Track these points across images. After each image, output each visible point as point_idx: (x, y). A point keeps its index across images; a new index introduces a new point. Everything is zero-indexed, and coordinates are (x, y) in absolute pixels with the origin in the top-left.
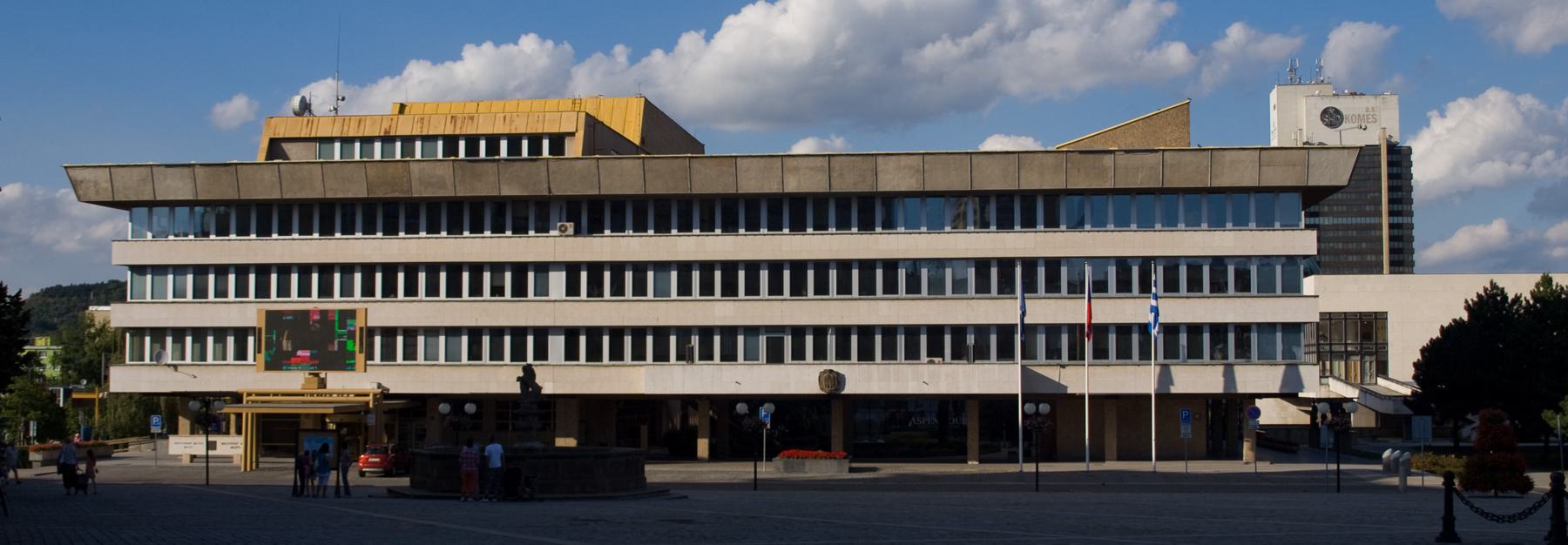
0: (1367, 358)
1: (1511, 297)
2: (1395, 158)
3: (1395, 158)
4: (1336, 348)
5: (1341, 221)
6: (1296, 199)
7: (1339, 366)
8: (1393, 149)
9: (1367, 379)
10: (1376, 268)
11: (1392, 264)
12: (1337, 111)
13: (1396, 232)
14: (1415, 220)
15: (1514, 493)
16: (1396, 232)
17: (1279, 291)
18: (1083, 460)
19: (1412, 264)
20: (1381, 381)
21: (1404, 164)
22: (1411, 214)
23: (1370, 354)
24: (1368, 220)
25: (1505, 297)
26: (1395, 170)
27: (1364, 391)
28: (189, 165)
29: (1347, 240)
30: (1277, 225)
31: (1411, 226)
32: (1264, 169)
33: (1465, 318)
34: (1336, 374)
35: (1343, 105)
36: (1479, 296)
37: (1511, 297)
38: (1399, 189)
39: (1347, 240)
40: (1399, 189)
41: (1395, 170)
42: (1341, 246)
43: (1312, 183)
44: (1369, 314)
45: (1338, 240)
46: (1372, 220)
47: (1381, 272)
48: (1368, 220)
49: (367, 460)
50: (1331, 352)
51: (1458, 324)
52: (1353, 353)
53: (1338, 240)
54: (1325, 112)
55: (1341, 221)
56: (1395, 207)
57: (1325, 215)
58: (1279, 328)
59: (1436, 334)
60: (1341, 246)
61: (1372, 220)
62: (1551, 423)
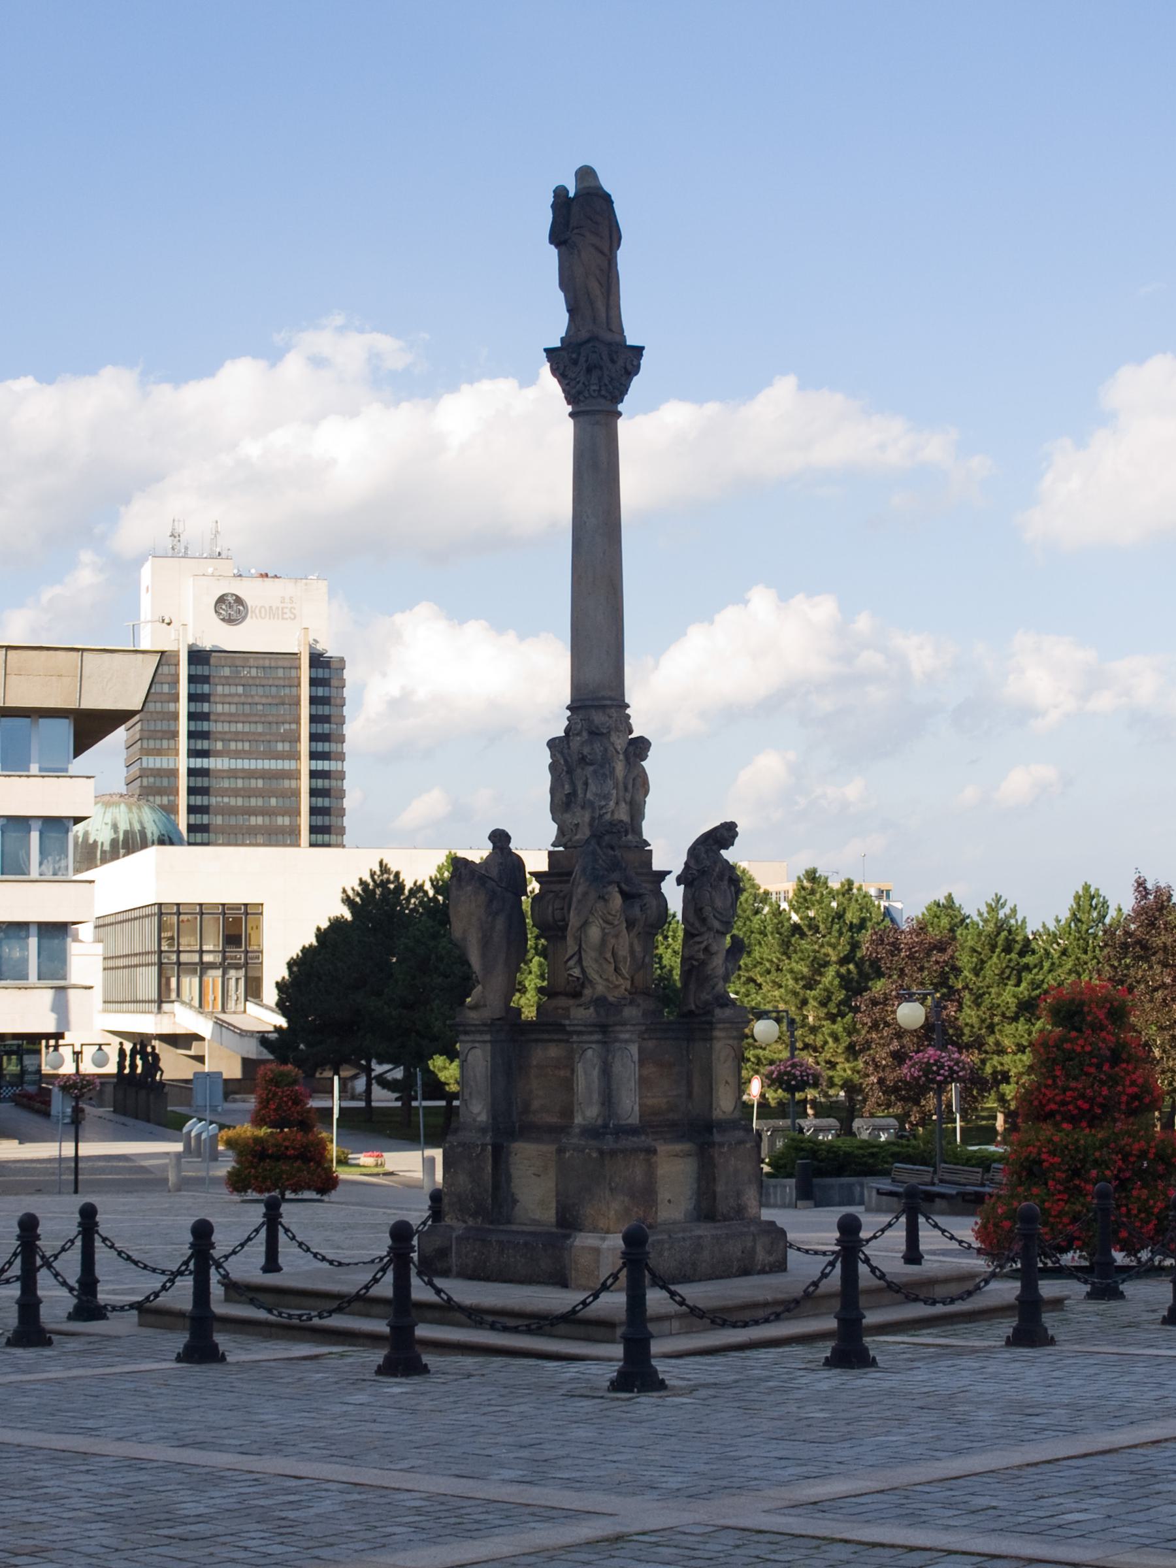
0: (232, 973)
1: (409, 885)
2: (321, 673)
3: (321, 673)
4: (184, 958)
5: (240, 764)
6: (64, 730)
7: (190, 984)
8: (317, 660)
9: (231, 1005)
10: (289, 837)
11: (313, 830)
12: (239, 600)
13: (320, 783)
14: (348, 766)
15: (312, 1195)
16: (320, 783)
17: (34, 873)
18: (425, 1108)
19: (341, 831)
20: (251, 1007)
21: (334, 682)
22: (341, 757)
23: (237, 967)
24: (279, 765)
25: (400, 887)
26: (320, 692)
27: (220, 1024)
28: (77, 650)
29: (248, 793)
30: (34, 768)
31: (341, 776)
32: (12, 679)
33: (348, 916)
34: (185, 996)
35: (246, 590)
36: (362, 883)
37: (409, 885)
38: (326, 719)
39: (248, 793)
40: (326, 719)
41: (320, 692)
42: (240, 802)
43: (87, 704)
44: (236, 907)
45: (236, 793)
46: (287, 765)
47: (297, 844)
48: (279, 765)
49: (447, 1071)
50: (179, 964)
51: (337, 925)
52: (212, 966)
53: (236, 793)
54: (221, 600)
55: (240, 764)
56: (320, 747)
57: (218, 754)
58: (33, 930)
59: (311, 940)
60: (240, 802)
61: (287, 765)
62: (442, 1076)
